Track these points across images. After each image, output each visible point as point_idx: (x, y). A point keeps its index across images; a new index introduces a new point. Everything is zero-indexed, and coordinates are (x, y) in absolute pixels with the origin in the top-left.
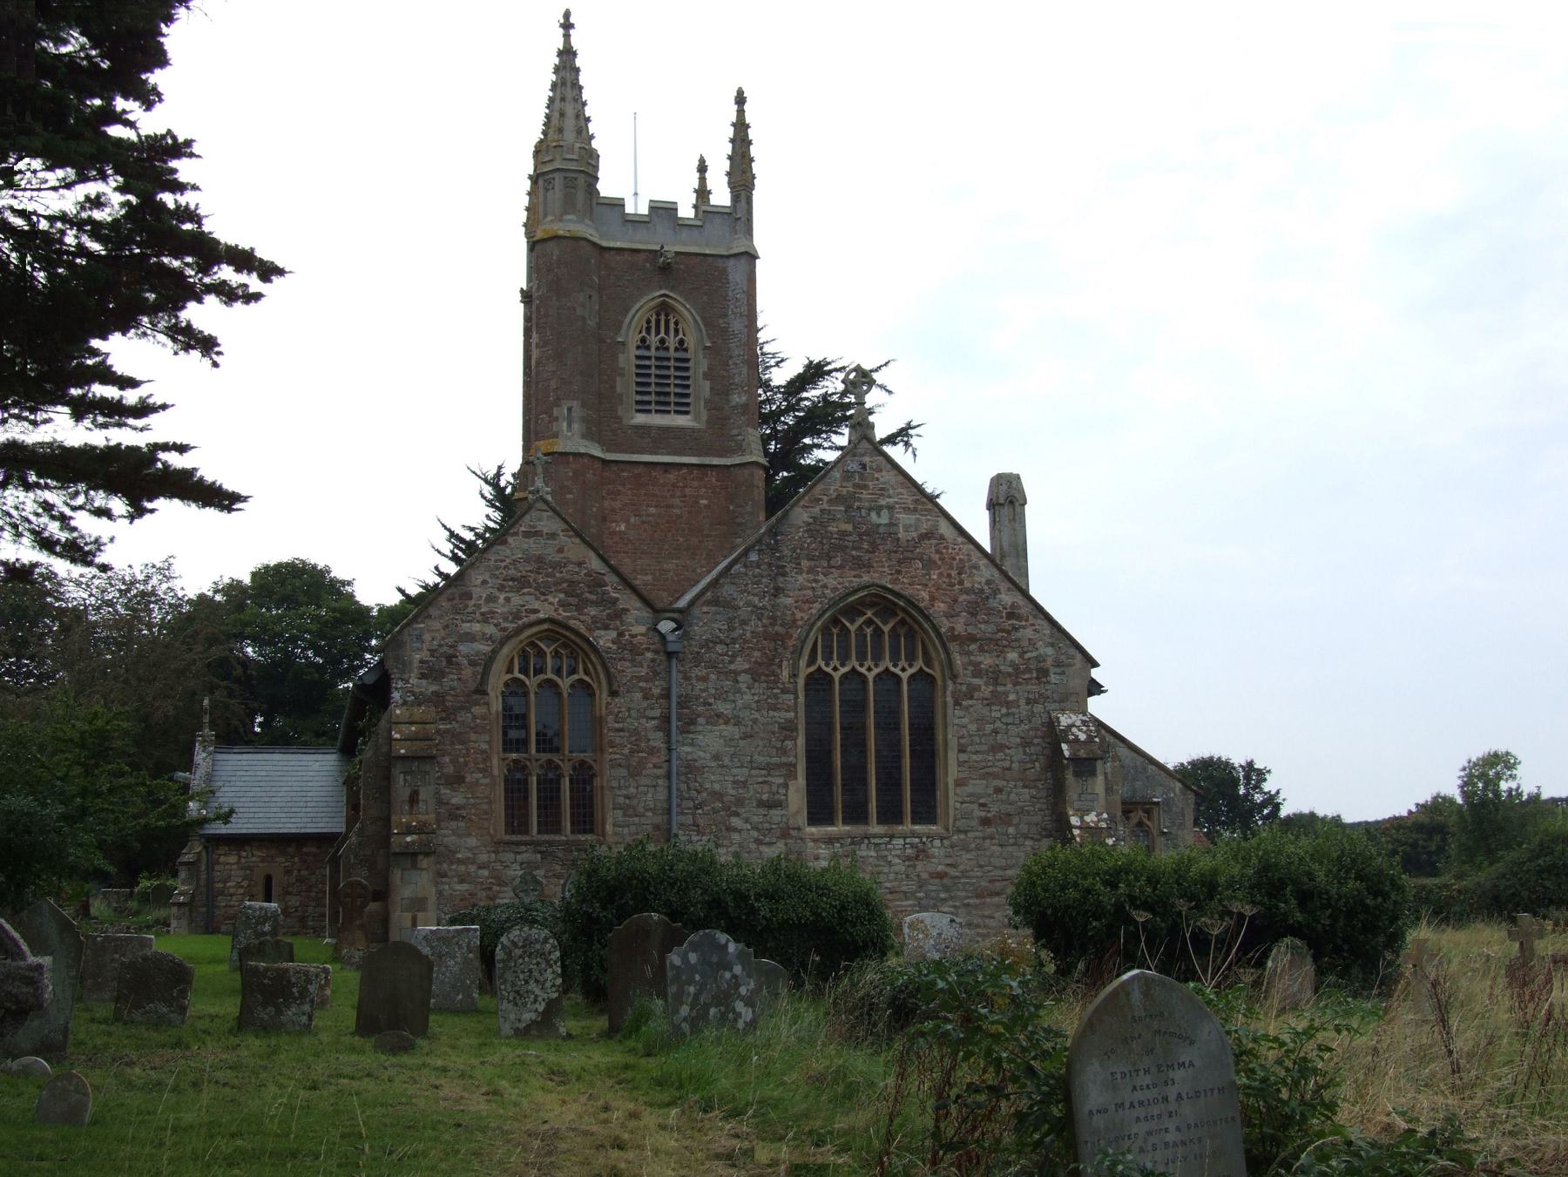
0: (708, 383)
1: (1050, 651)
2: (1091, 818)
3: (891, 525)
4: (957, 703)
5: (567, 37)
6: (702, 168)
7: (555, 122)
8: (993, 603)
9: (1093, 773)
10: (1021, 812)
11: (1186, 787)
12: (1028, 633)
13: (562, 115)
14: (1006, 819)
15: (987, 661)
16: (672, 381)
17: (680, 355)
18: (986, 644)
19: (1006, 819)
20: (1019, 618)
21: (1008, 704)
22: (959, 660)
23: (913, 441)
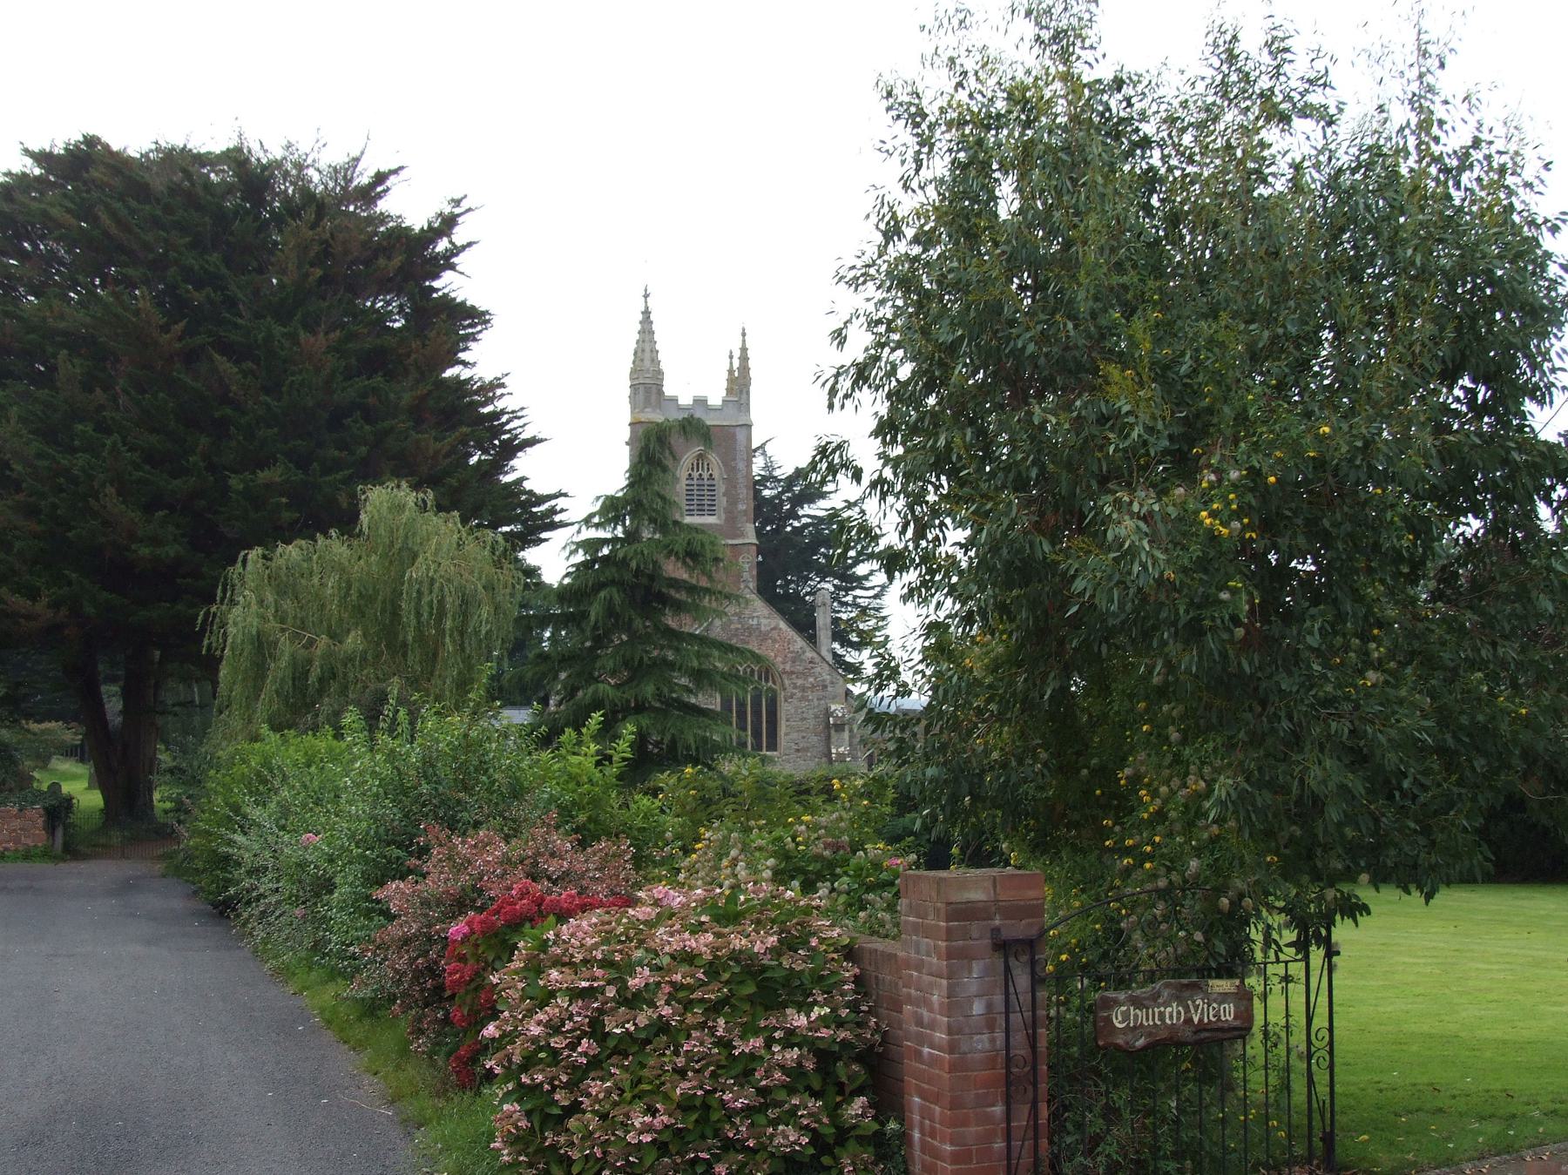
3: (759, 624)
6: (731, 357)
7: (639, 354)
10: (813, 746)
13: (643, 351)
14: (806, 750)
15: (799, 682)
17: (710, 482)
18: (799, 675)
19: (806, 750)
22: (787, 682)
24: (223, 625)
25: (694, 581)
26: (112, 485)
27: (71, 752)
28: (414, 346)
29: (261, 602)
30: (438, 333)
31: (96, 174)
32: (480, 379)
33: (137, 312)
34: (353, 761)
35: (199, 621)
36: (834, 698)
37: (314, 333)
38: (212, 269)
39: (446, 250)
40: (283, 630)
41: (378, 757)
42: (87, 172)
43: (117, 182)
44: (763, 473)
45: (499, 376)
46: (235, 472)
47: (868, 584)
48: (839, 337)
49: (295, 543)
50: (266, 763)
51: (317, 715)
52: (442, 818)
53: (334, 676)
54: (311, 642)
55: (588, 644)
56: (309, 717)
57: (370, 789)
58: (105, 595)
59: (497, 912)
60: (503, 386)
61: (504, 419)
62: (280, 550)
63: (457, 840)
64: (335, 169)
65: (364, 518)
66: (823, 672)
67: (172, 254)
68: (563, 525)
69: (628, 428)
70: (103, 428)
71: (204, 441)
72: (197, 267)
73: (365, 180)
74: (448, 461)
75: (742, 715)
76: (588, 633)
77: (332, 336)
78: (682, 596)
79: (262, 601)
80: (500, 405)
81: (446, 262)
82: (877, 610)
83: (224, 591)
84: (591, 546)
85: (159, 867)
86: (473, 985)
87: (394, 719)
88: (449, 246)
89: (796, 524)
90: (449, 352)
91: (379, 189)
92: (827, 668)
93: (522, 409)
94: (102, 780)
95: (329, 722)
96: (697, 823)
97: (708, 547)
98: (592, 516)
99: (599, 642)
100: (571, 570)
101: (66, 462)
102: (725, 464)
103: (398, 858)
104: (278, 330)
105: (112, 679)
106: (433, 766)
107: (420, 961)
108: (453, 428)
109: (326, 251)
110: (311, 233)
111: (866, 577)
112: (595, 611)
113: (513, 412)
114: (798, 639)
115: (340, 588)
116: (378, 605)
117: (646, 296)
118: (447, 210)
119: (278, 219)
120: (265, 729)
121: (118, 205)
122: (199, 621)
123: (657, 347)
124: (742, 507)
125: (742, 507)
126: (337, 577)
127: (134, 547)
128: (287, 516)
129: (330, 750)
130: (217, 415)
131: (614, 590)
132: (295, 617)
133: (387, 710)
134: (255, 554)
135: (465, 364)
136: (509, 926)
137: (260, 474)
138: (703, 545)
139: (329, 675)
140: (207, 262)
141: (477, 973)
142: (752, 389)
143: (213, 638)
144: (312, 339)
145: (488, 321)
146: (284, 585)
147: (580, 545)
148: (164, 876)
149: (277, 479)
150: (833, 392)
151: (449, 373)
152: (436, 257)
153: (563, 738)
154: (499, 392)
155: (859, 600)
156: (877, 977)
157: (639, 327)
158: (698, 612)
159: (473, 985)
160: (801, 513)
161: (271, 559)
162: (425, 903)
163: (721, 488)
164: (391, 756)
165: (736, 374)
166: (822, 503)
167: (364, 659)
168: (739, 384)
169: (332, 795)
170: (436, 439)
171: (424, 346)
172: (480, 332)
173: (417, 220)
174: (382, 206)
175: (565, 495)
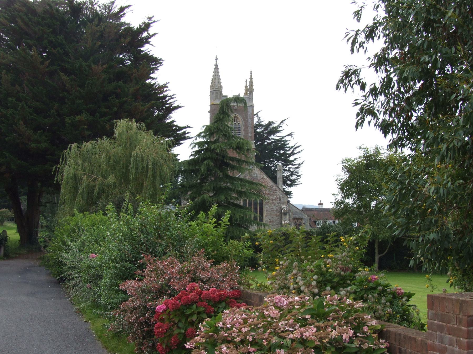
0: (244, 132)
1: (281, 196)
2: (286, 222)
4: (266, 204)
5: (216, 61)
6: (246, 82)
8: (272, 188)
9: (287, 215)
11: (308, 216)
12: (278, 193)
13: (215, 79)
15: (271, 197)
16: (237, 130)
17: (238, 126)
20: (276, 191)
21: (274, 204)
23: (293, 135)
24: (62, 172)
25: (239, 158)
26: (22, 120)
27: (11, 220)
28: (134, 71)
29: (76, 164)
30: (143, 66)
31: (16, 6)
32: (158, 84)
33: (32, 56)
34: (111, 224)
35: (53, 171)
36: (283, 204)
37: (98, 65)
38: (60, 41)
39: (146, 36)
40: (85, 174)
41: (121, 223)
42: (13, 5)
43: (24, 9)
44: (257, 123)
45: (165, 83)
46: (68, 116)
47: (294, 163)
48: (358, 14)
49: (90, 142)
50: (76, 225)
51: (97, 206)
52: (151, 252)
53: (104, 192)
54: (95, 179)
55: (199, 181)
56: (94, 207)
57: (118, 237)
58: (19, 161)
59: (180, 299)
60: (167, 87)
61: (167, 99)
62: (84, 144)
63: (158, 263)
64: (105, 6)
65: (116, 132)
66: (280, 194)
67: (45, 36)
68: (188, 138)
69: (210, 107)
70: (19, 100)
71: (56, 105)
72: (54, 41)
73: (116, 10)
74: (147, 113)
75: (256, 209)
76: (199, 177)
77: (104, 66)
78: (235, 164)
79: (77, 163)
80: (165, 94)
81: (146, 41)
82: (297, 172)
83: (63, 159)
84: (200, 144)
85: (39, 262)
86: (168, 334)
87: (127, 208)
88: (147, 35)
89: (268, 141)
90: (147, 73)
91: (121, 14)
92: (281, 192)
93: (174, 95)
94: (20, 231)
95: (101, 209)
96: (274, 256)
97: (245, 145)
98: (201, 133)
99: (203, 181)
100: (193, 153)
101: (5, 112)
102: (244, 120)
103: (130, 268)
104: (84, 64)
105: (24, 194)
106: (146, 227)
107: (141, 318)
108: (148, 102)
109: (102, 36)
110: (96, 28)
111: (293, 161)
112: (203, 168)
113: (170, 96)
114: (271, 182)
115: (106, 159)
116: (121, 165)
117: (216, 59)
118: (147, 21)
119: (84, 23)
120: (75, 211)
121: (25, 17)
122: (53, 171)
123: (220, 78)
124: (250, 135)
125: (250, 135)
126: (105, 154)
127: (29, 143)
128: (87, 133)
129: (102, 220)
130: (61, 95)
131: (210, 161)
132: (89, 169)
133: (124, 204)
134: (74, 146)
135: (153, 78)
136: (186, 306)
137: (77, 117)
138: (243, 144)
139: (102, 192)
140: (58, 39)
141: (170, 328)
142: (254, 93)
143: (58, 177)
144: (97, 67)
145: (161, 63)
146: (85, 157)
147: (196, 144)
148: (40, 266)
149: (84, 119)
150: (354, 43)
151: (147, 82)
152: (142, 39)
153: (199, 216)
154: (165, 89)
155: (291, 169)
156: (400, 349)
157: (214, 70)
158: (240, 169)
159: (168, 334)
160: (270, 138)
161: (80, 148)
162: (144, 291)
163: (242, 128)
164: (127, 223)
165: (248, 88)
166: (278, 134)
167: (115, 186)
168: (249, 90)
169: (102, 238)
170: (142, 106)
171: (138, 71)
172: (159, 67)
173: (135, 25)
174: (123, 20)
175: (189, 127)
